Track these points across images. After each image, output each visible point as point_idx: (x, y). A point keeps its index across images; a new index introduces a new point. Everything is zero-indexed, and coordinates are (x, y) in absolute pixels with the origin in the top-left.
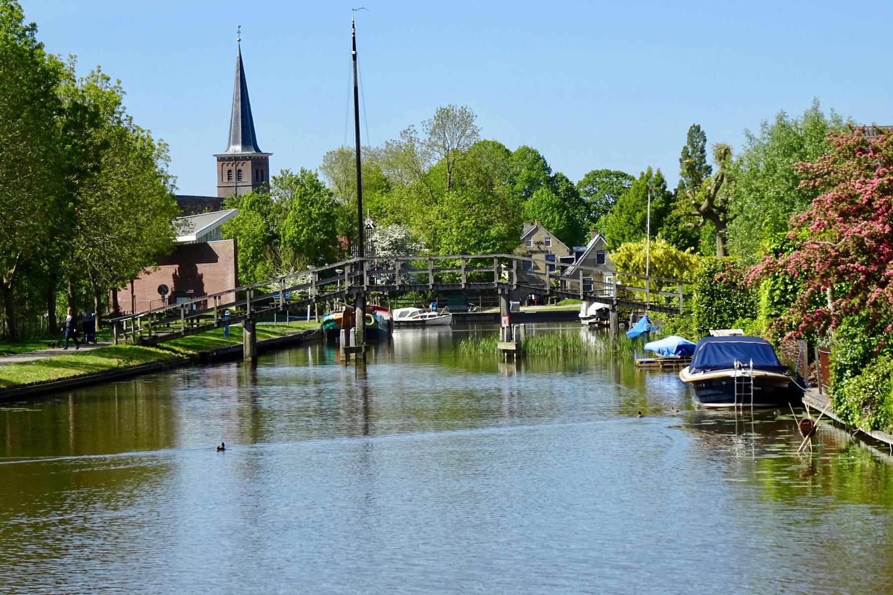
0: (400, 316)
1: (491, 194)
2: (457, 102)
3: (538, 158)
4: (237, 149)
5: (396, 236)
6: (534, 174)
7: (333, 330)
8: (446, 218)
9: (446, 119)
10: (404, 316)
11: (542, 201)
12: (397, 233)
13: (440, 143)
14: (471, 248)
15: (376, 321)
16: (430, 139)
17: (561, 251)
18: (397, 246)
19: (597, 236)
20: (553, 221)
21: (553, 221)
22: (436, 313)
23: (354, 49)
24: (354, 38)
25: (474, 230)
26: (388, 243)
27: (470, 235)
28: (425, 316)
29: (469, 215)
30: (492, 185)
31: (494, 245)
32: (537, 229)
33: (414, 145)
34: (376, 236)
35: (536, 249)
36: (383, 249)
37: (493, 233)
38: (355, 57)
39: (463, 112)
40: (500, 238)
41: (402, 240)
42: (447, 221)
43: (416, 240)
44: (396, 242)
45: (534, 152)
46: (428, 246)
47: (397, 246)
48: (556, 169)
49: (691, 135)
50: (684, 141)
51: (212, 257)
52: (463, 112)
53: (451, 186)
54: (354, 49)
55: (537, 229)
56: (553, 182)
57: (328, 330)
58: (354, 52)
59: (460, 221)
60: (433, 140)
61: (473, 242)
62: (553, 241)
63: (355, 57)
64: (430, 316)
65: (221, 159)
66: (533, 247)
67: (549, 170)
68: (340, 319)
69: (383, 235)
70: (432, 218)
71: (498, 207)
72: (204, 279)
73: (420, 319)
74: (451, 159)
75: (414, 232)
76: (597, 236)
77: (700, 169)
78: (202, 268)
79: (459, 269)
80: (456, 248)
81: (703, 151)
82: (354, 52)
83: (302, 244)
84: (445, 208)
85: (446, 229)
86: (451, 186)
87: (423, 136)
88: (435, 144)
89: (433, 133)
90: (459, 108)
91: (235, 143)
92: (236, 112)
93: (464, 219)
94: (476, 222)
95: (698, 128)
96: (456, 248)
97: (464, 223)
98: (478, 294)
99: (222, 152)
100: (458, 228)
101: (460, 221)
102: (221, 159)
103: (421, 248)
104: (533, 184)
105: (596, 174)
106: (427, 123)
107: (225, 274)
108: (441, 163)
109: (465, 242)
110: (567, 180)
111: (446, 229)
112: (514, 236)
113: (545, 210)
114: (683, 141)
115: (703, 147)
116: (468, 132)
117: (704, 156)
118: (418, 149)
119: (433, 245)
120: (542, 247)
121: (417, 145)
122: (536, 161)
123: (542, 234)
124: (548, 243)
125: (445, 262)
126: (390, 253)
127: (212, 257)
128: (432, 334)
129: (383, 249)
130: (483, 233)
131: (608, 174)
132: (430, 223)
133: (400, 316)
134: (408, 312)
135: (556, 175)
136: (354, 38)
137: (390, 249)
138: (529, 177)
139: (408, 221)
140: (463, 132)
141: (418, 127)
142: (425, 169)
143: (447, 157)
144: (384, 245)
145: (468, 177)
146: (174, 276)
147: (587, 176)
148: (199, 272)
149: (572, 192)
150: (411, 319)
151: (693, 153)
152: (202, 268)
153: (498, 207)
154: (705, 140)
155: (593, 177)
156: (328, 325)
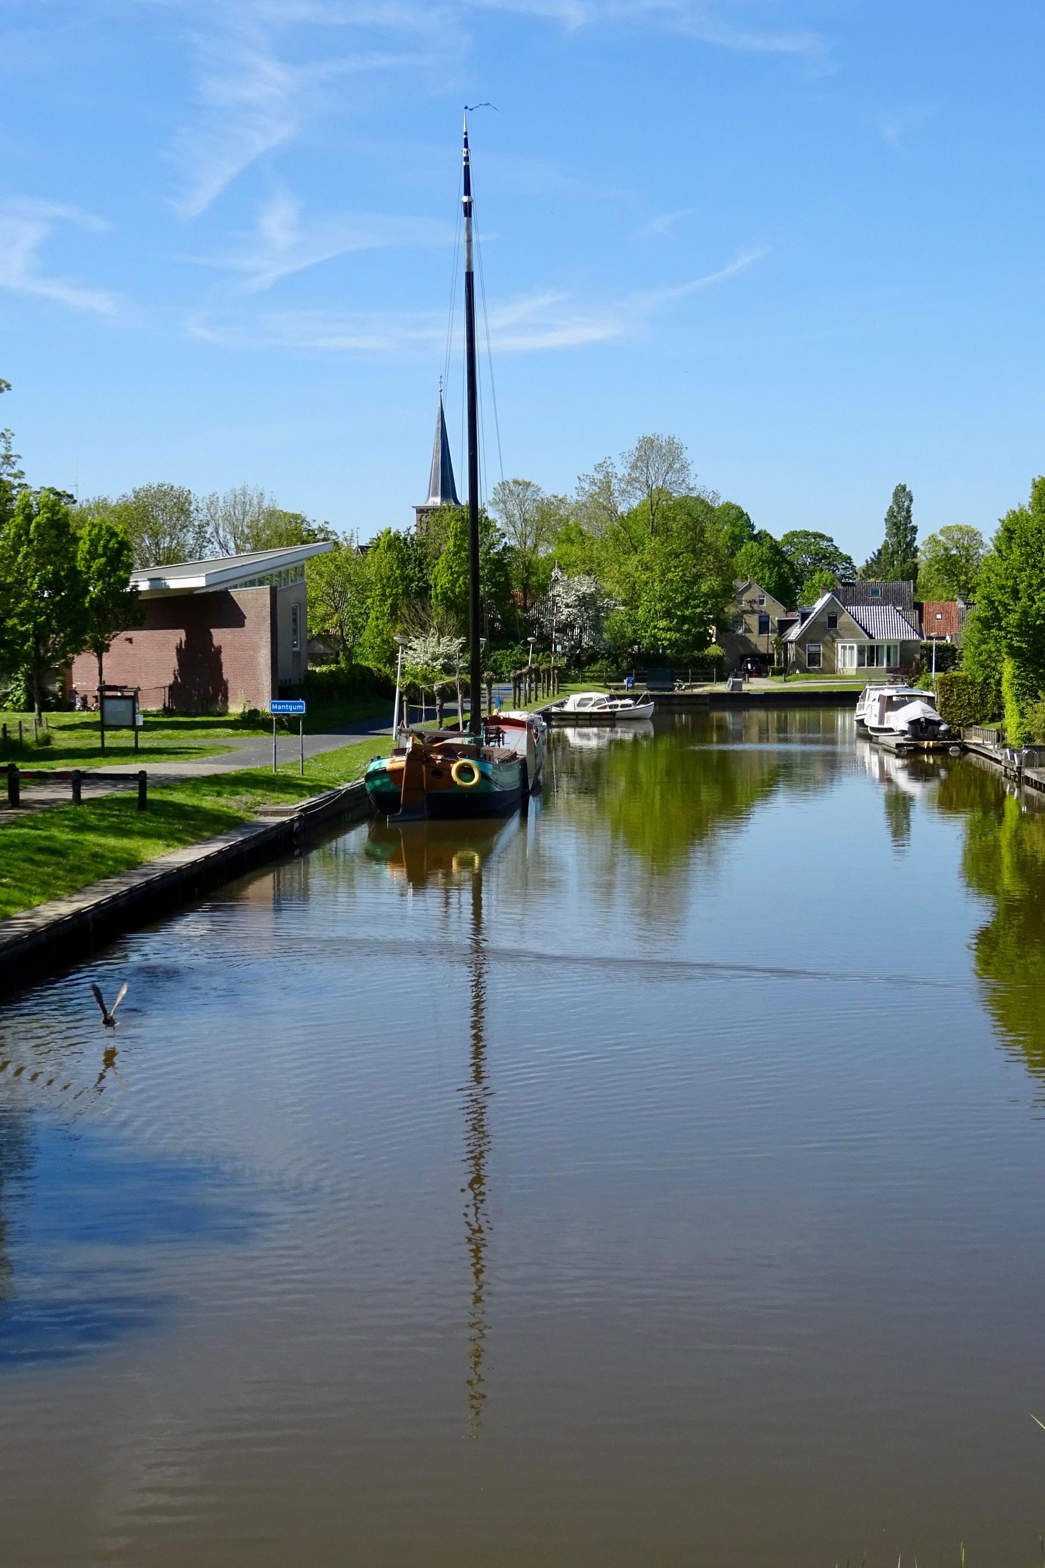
0: (579, 705)
1: (702, 542)
2: (663, 430)
3: (741, 515)
4: (436, 501)
5: (584, 589)
6: (737, 531)
7: (386, 794)
8: (647, 569)
9: (652, 452)
10: (585, 705)
11: (752, 557)
12: (585, 586)
13: (643, 479)
14: (677, 606)
15: (483, 775)
16: (629, 475)
17: (777, 613)
18: (585, 602)
19: (828, 596)
20: (762, 578)
21: (762, 578)
22: (631, 702)
23: (467, 192)
24: (467, 169)
25: (681, 584)
26: (573, 598)
27: (676, 591)
28: (616, 706)
29: (675, 567)
30: (703, 531)
31: (706, 603)
32: (749, 587)
33: (610, 482)
34: (559, 589)
35: (748, 608)
36: (567, 606)
37: (704, 588)
38: (468, 209)
39: (671, 442)
40: (713, 594)
41: (592, 594)
42: (648, 574)
43: (609, 595)
44: (584, 597)
45: (738, 508)
46: (624, 603)
47: (585, 603)
48: (760, 525)
49: (896, 495)
50: (889, 501)
51: (234, 618)
52: (671, 442)
53: (655, 531)
54: (467, 192)
55: (749, 587)
56: (761, 538)
57: (376, 792)
58: (465, 199)
59: (664, 574)
60: (633, 475)
61: (679, 599)
62: (768, 599)
63: (468, 209)
64: (623, 706)
65: (421, 511)
66: (744, 606)
67: (753, 527)
68: (401, 770)
69: (568, 588)
70: (630, 569)
71: (710, 558)
72: (223, 656)
73: (608, 710)
74: (655, 497)
75: (608, 586)
76: (828, 596)
77: (905, 529)
78: (220, 636)
79: (663, 633)
80: (658, 607)
81: (908, 511)
82: (465, 199)
83: (456, 597)
84: (647, 558)
85: (647, 583)
86: (655, 531)
87: (621, 470)
88: (636, 480)
89: (634, 467)
90: (665, 437)
91: (435, 495)
92: (436, 463)
93: (669, 571)
94: (684, 575)
95: (904, 488)
96: (658, 607)
97: (670, 575)
98: (686, 666)
99: (421, 504)
100: (661, 581)
101: (664, 574)
102: (421, 511)
103: (615, 605)
104: (737, 541)
105: (794, 534)
106: (627, 455)
107: (256, 648)
108: (643, 504)
109: (671, 599)
110: (771, 538)
111: (647, 583)
112: (728, 592)
113: (754, 566)
114: (888, 501)
115: (909, 507)
116: (677, 466)
117: (910, 517)
118: (615, 485)
119: (631, 602)
120: (755, 606)
121: (614, 481)
122: (741, 519)
123: (755, 593)
124: (762, 602)
125: (644, 623)
126: (575, 611)
127: (234, 618)
128: (625, 734)
129: (567, 606)
130: (692, 588)
131: (806, 534)
132: (628, 575)
133: (579, 705)
134: (591, 699)
135: (760, 533)
136: (467, 169)
137: (575, 607)
138: (733, 532)
139: (602, 572)
140: (671, 467)
141: (617, 460)
142: (622, 509)
143: (650, 496)
144: (569, 601)
145: (674, 519)
146: (179, 650)
147: (785, 536)
148: (216, 643)
149: (775, 548)
150: (595, 710)
151: (898, 513)
152: (220, 636)
153: (710, 558)
154: (911, 500)
155: (792, 537)
156: (378, 782)
